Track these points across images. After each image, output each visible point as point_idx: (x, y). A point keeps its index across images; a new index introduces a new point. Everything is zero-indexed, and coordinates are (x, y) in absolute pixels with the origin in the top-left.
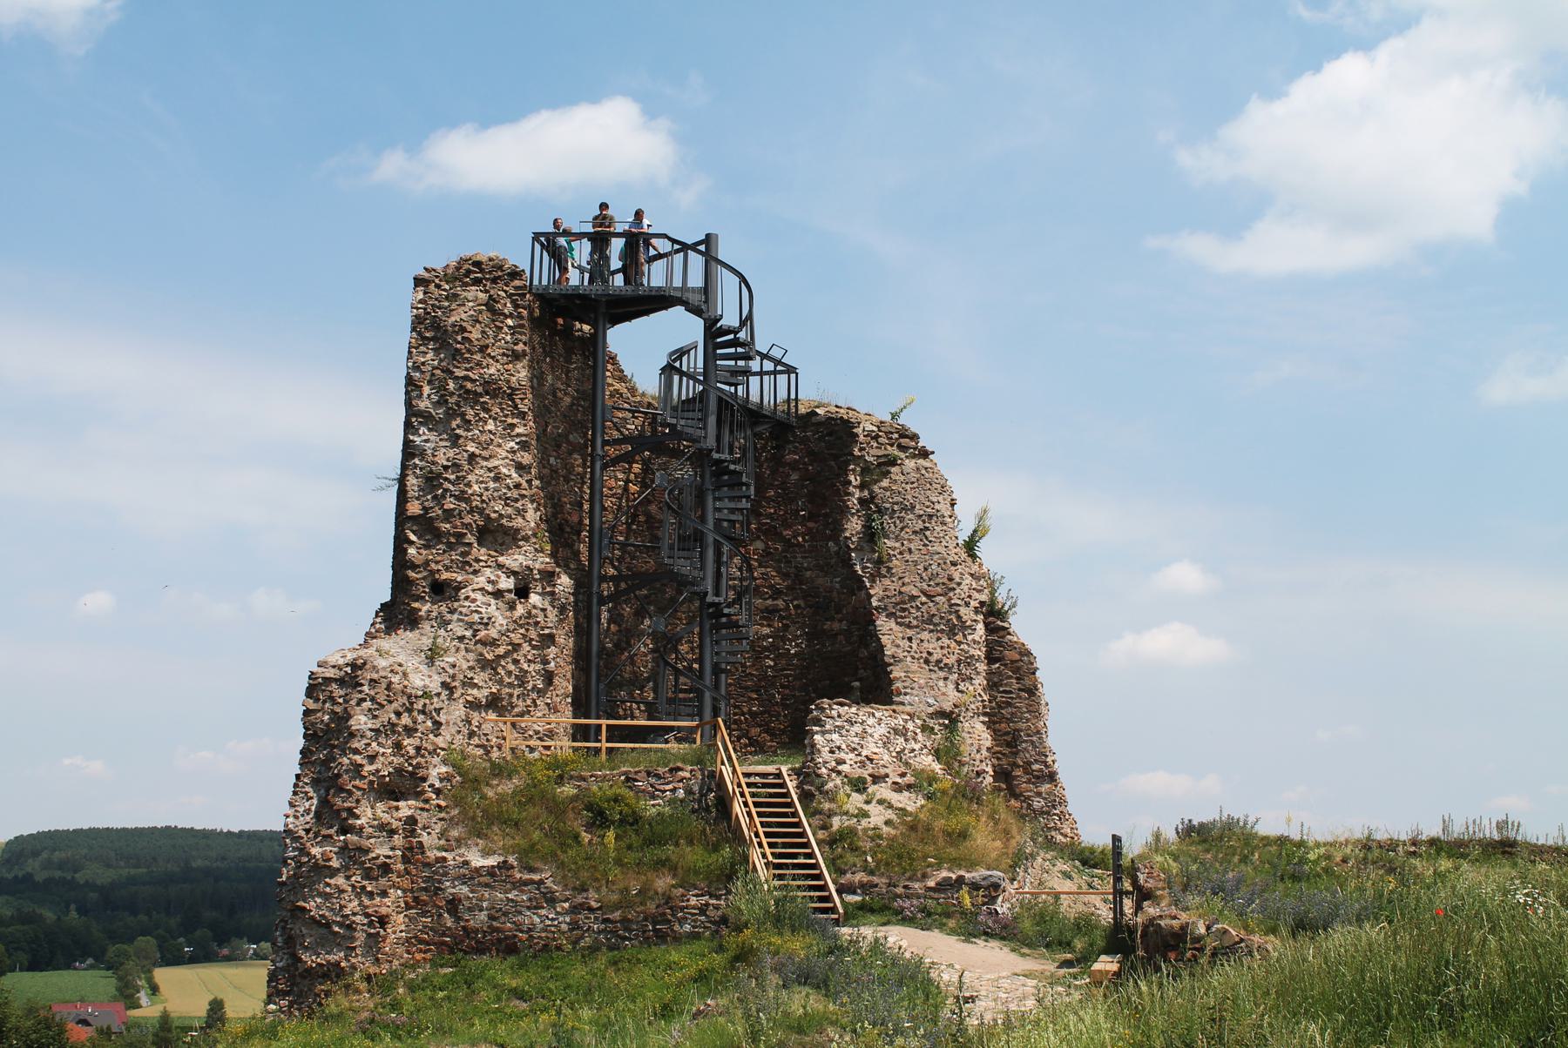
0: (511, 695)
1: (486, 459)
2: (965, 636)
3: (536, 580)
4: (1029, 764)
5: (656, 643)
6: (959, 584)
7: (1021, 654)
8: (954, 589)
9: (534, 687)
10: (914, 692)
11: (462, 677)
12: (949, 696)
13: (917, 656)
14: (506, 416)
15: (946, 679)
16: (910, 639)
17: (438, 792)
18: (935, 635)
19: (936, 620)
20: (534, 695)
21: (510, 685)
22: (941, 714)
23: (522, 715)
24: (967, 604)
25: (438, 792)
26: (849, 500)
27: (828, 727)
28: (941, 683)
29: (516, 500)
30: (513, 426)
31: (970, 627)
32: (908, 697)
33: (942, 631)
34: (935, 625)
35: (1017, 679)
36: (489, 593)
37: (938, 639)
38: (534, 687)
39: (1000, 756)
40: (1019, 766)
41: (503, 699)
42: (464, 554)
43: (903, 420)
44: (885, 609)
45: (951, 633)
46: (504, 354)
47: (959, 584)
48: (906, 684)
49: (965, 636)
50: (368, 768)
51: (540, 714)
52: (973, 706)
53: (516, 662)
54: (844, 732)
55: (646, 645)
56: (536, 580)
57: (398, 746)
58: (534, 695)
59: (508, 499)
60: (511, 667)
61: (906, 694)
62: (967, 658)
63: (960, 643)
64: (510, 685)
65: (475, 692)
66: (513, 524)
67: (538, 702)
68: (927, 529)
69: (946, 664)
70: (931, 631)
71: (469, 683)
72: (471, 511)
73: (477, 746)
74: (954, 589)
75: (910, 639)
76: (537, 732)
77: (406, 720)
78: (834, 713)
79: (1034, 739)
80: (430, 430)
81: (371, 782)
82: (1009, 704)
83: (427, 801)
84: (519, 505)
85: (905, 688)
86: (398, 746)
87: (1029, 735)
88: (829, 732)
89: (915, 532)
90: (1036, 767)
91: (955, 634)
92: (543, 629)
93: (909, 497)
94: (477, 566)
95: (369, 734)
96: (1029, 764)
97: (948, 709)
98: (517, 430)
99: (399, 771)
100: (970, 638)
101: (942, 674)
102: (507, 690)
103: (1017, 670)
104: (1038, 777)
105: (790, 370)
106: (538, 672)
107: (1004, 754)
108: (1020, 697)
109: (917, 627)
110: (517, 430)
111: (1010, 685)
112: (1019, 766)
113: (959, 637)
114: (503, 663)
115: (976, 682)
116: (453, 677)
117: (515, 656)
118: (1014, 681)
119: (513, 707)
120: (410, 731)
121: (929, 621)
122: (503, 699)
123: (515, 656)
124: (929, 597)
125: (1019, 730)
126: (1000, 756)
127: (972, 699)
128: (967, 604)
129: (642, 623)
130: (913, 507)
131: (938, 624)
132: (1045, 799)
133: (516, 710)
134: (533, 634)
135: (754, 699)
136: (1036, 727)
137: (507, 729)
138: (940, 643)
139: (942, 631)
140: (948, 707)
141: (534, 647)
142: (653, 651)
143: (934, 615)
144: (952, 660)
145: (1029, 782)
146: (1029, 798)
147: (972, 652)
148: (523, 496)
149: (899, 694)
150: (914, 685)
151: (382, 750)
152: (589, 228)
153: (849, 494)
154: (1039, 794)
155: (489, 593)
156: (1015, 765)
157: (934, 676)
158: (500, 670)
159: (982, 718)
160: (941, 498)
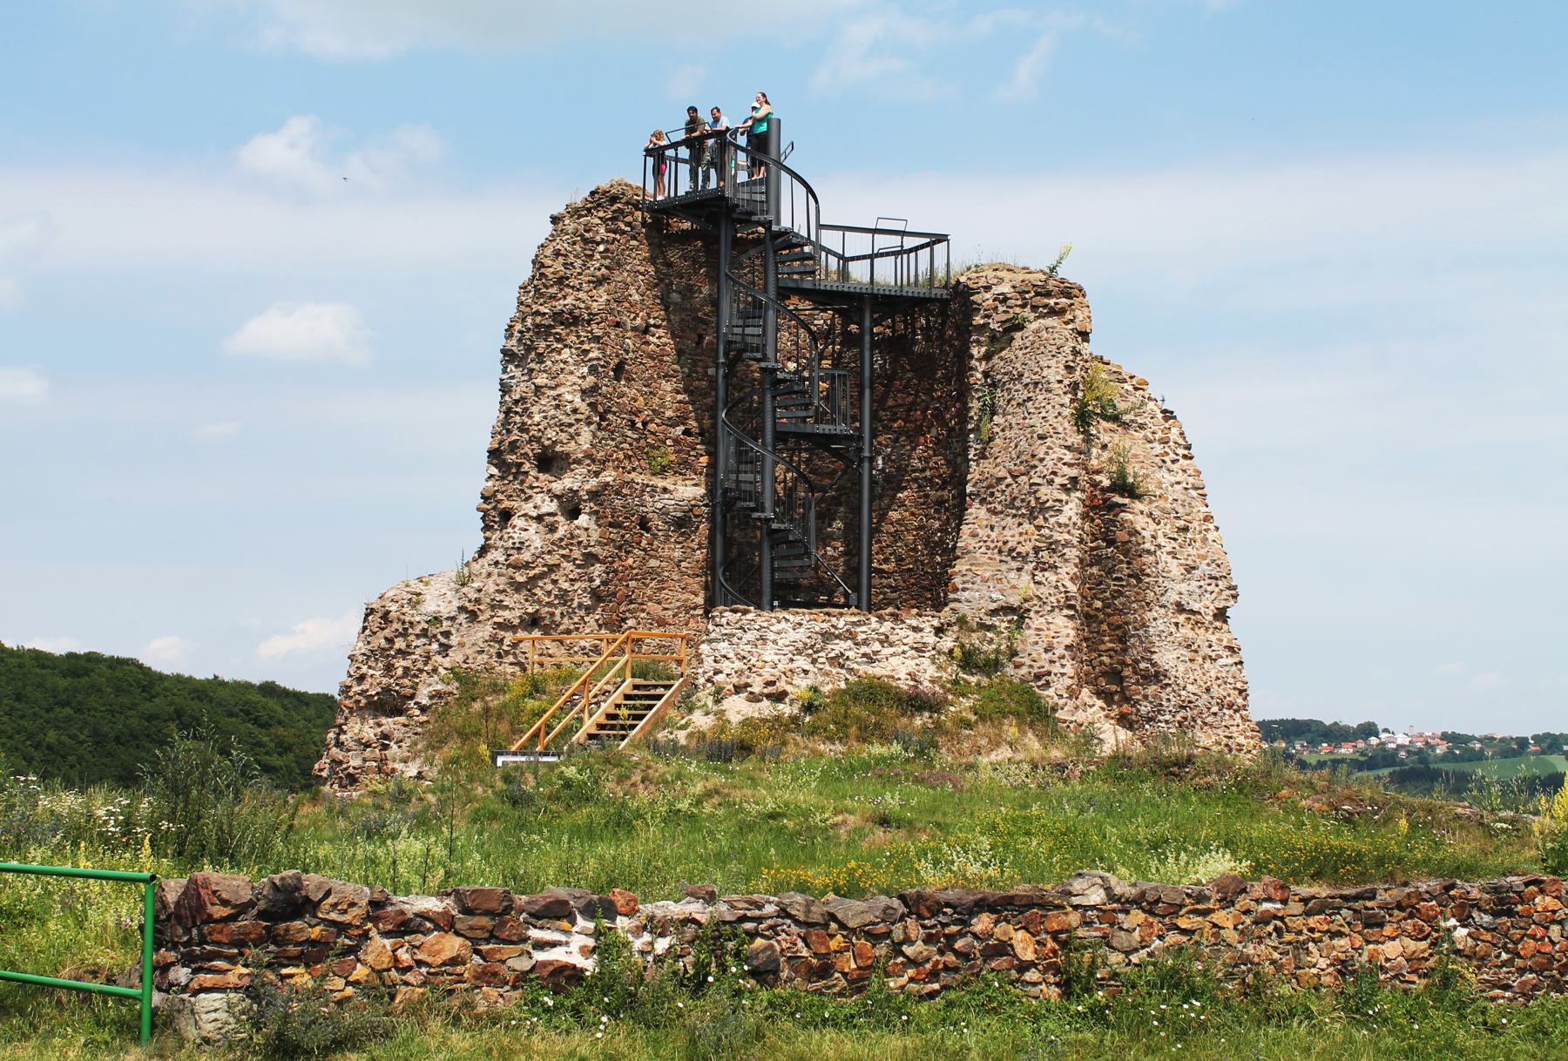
0: (553, 614)
1: (551, 388)
2: (1046, 519)
3: (585, 501)
4: (1136, 662)
5: (847, 546)
6: (1042, 460)
7: (1131, 534)
8: (1036, 467)
9: (580, 605)
10: (975, 586)
11: (488, 600)
12: (1020, 585)
13: (992, 545)
14: (582, 343)
15: (1019, 570)
16: (992, 528)
17: (423, 709)
18: (1017, 521)
19: (1018, 503)
20: (582, 613)
21: (549, 604)
22: (1007, 609)
23: (568, 632)
24: (1051, 482)
25: (423, 709)
26: (972, 376)
27: (713, 635)
28: (1013, 575)
29: (570, 425)
30: (586, 352)
31: (1051, 508)
32: (966, 594)
33: (1023, 515)
34: (1018, 509)
35: (1129, 563)
36: (532, 518)
37: (1020, 524)
38: (580, 605)
39: (1112, 653)
40: (1128, 665)
41: (544, 618)
42: (522, 482)
43: (1062, 273)
44: (978, 495)
45: (1032, 517)
46: (589, 282)
47: (1042, 460)
48: (965, 579)
49: (1046, 519)
50: (356, 689)
51: (588, 631)
52: (1053, 599)
53: (555, 582)
54: (735, 640)
55: (835, 548)
56: (585, 501)
57: (389, 668)
58: (582, 613)
59: (562, 425)
60: (549, 587)
61: (964, 590)
62: (1051, 544)
63: (1039, 528)
64: (549, 604)
65: (507, 614)
66: (566, 448)
67: (586, 619)
68: (1030, 399)
69: (1019, 553)
70: (1014, 516)
71: (496, 606)
72: (529, 442)
73: (511, 664)
74: (1036, 467)
75: (992, 528)
76: (583, 648)
77: (400, 644)
78: (724, 621)
79: (1141, 632)
80: (517, 367)
81: (358, 702)
82: (1121, 593)
83: (411, 717)
84: (572, 430)
85: (964, 583)
86: (389, 668)
87: (1136, 629)
88: (716, 640)
89: (1019, 404)
90: (1143, 665)
91: (1035, 518)
92: (586, 548)
93: (1018, 365)
94: (529, 492)
95: (361, 658)
96: (1136, 662)
97: (1016, 604)
98: (591, 355)
99: (387, 690)
100: (1052, 520)
101: (1014, 565)
102: (547, 609)
103: (1126, 553)
104: (1144, 677)
105: (941, 238)
106: (585, 590)
107: (1116, 651)
108: (1129, 584)
109: (1002, 512)
110: (591, 355)
111: (1120, 570)
112: (1128, 665)
113: (1040, 521)
114: (541, 584)
115: (1063, 571)
116: (478, 601)
117: (553, 576)
118: (1125, 566)
119: (558, 626)
120: (403, 653)
121: (1011, 505)
122: (544, 618)
123: (553, 576)
124: (1014, 477)
125: (1127, 623)
126: (1112, 653)
127: (1052, 591)
128: (1051, 482)
129: (830, 526)
130: (1021, 375)
131: (1018, 509)
132: (1151, 703)
133: (562, 627)
134: (577, 553)
135: (928, 599)
136: (1143, 619)
137: (553, 648)
138: (1020, 530)
139: (1023, 515)
140: (1015, 601)
141: (579, 566)
142: (844, 554)
143: (1015, 498)
144: (1027, 548)
145: (1137, 683)
146: (1137, 702)
147: (1057, 536)
148: (578, 421)
149: (956, 590)
150: (978, 580)
151: (371, 672)
152: (681, 136)
153: (972, 369)
154: (1146, 697)
155: (532, 518)
156: (1123, 663)
157: (1004, 567)
158: (538, 591)
159: (1066, 612)
160: (1053, 363)
